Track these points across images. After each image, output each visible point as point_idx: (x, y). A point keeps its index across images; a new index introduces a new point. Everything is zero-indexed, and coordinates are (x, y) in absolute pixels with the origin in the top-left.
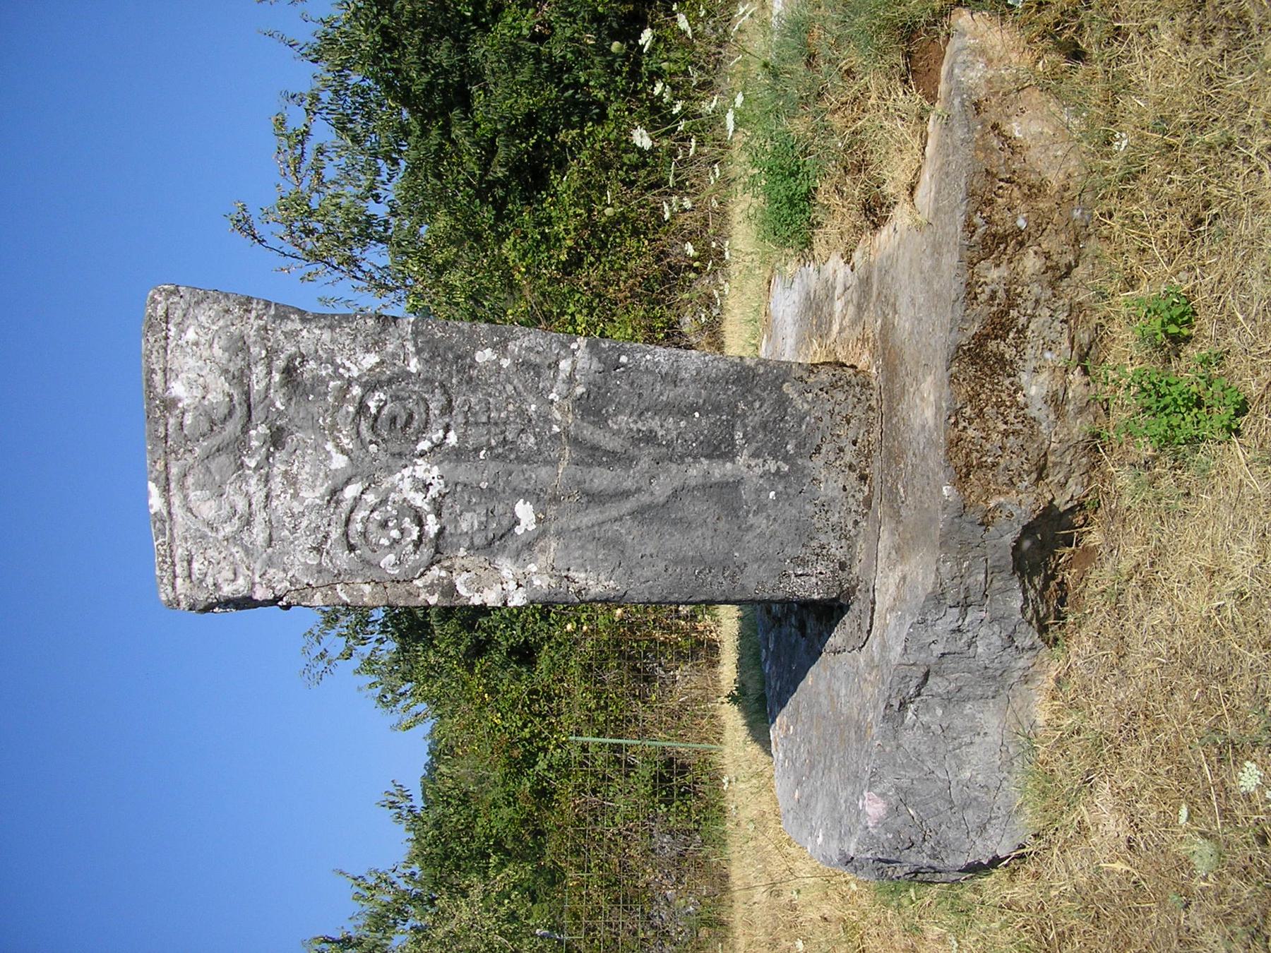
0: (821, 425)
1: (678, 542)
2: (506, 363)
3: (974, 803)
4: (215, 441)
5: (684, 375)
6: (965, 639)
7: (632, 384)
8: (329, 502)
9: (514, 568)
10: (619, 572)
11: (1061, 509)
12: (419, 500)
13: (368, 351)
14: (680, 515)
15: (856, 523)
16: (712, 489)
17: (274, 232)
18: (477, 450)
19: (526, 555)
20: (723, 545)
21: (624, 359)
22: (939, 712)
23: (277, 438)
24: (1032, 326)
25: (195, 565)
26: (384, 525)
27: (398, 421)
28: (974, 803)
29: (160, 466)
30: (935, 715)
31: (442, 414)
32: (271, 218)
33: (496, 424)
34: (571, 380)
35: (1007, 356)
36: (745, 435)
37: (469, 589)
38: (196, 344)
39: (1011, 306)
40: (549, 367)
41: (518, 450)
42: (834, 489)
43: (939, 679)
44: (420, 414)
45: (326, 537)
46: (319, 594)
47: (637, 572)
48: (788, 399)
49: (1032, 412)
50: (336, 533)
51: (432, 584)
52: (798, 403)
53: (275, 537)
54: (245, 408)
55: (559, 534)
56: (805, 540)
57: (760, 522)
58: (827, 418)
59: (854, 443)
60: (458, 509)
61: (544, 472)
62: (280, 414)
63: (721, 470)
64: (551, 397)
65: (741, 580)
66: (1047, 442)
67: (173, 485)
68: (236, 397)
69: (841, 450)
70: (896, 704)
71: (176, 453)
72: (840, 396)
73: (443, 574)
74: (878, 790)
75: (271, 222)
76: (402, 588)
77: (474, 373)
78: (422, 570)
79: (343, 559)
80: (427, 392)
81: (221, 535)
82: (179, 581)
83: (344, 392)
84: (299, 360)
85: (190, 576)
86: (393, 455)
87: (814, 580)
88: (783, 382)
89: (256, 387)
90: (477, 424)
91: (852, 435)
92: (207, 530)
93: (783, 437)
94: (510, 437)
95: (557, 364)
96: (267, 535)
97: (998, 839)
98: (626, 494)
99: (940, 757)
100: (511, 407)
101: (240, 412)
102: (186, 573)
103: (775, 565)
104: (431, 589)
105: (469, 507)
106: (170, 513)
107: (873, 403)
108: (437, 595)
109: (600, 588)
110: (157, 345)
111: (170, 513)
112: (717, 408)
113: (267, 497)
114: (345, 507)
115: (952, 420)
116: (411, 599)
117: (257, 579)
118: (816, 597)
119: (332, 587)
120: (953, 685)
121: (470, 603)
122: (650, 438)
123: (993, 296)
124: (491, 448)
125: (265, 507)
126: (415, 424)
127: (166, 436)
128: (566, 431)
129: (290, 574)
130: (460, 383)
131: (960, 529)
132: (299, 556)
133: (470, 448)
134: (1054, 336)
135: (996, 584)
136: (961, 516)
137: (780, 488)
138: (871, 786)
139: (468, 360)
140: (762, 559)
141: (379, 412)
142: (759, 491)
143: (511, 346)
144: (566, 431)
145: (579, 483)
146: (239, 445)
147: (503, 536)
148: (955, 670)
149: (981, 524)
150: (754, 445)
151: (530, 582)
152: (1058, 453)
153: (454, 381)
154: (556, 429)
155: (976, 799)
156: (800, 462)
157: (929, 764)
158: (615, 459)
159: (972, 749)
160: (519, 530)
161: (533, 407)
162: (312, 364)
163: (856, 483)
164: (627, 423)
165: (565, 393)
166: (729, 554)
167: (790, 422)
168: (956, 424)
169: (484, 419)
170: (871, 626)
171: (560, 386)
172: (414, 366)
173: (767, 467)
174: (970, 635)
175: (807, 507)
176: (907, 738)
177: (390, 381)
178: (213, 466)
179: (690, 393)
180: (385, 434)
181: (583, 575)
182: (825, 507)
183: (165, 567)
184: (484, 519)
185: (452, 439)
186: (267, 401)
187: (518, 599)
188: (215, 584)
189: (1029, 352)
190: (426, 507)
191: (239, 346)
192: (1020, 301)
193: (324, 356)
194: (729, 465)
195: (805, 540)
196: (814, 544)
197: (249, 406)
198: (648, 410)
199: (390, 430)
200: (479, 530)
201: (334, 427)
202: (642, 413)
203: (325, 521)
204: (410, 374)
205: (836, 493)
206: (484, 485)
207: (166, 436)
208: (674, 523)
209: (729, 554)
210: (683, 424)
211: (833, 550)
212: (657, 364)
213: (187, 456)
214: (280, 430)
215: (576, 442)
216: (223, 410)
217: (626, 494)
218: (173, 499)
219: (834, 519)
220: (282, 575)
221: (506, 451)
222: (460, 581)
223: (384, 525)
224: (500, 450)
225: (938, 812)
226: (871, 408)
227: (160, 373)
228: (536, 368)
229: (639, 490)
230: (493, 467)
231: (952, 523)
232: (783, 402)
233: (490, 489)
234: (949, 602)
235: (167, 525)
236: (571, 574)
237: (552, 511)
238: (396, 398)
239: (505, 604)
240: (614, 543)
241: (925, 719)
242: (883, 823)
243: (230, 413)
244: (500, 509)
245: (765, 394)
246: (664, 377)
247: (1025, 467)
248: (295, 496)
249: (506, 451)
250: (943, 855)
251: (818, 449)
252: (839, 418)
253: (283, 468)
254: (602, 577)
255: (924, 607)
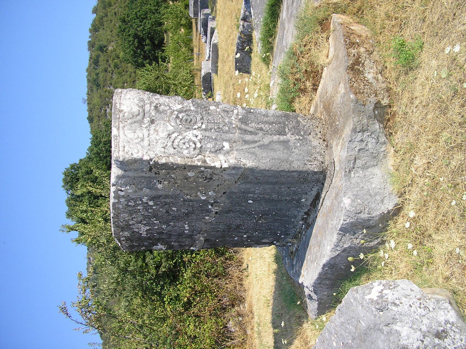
0: (310, 128)
1: (272, 154)
2: (218, 110)
3: (378, 194)
4: (134, 120)
5: (269, 115)
6: (365, 143)
7: (255, 116)
8: (167, 137)
9: (224, 158)
10: (255, 161)
11: (384, 105)
12: (194, 139)
13: (179, 104)
14: (272, 148)
15: (324, 152)
16: (280, 142)
17: (76, 314)
18: (211, 129)
19: (227, 155)
20: (286, 156)
21: (252, 111)
22: (361, 172)
23: (152, 122)
24: (366, 63)
25: (126, 148)
26: (184, 144)
27: (188, 121)
28: (378, 194)
29: (117, 124)
30: (360, 173)
31: (201, 119)
32: (75, 305)
33: (216, 123)
34: (237, 114)
35: (361, 70)
36: (289, 130)
37: (210, 162)
38: (130, 99)
39: (359, 58)
40: (231, 111)
41: (223, 130)
42: (316, 143)
43: (359, 160)
44: (194, 119)
45: (167, 145)
46: (164, 158)
47: (261, 161)
48: (299, 121)
49: (370, 81)
50: (170, 144)
51: (199, 159)
52: (303, 122)
53: (150, 144)
54: (143, 113)
55: (237, 150)
56: (310, 156)
57: (296, 151)
58: (311, 126)
59: (320, 132)
60: (206, 142)
61: (231, 135)
62: (153, 116)
63: (282, 138)
64: (232, 118)
65: (293, 165)
66: (376, 88)
67: (120, 129)
68: (141, 111)
69: (317, 134)
70: (347, 170)
71: (122, 122)
72: (314, 121)
73: (202, 157)
74: (347, 196)
75: (75, 307)
76: (189, 160)
77: (210, 111)
78: (196, 155)
79: (172, 151)
80: (196, 114)
81: (134, 142)
82: (120, 152)
83: (172, 113)
84: (159, 105)
85: (124, 151)
86: (187, 128)
87: (314, 166)
88: (298, 117)
89: (146, 109)
90: (211, 123)
91: (319, 130)
92: (130, 141)
93: (300, 130)
94: (221, 127)
95: (233, 111)
96: (148, 143)
97: (388, 203)
98: (256, 142)
99: (364, 183)
100: (220, 120)
101: (142, 114)
102: (123, 150)
103: (302, 162)
104: (199, 160)
105: (209, 142)
106: (119, 135)
107: (324, 123)
108: (200, 162)
109: (250, 165)
110: (118, 98)
111: (119, 135)
112: (280, 123)
113: (149, 134)
114: (172, 139)
115: (350, 82)
116: (192, 163)
117: (145, 154)
118: (316, 170)
119: (168, 157)
120: (364, 162)
121: (211, 165)
122: (261, 129)
123: (354, 55)
124: (215, 129)
125: (148, 137)
126: (193, 122)
127: (119, 118)
128: (237, 126)
129: (155, 153)
130: (206, 113)
131: (357, 107)
132: (158, 148)
133: (209, 128)
134: (372, 66)
135: (370, 123)
136: (357, 103)
137: (301, 142)
138: (345, 196)
139: (208, 108)
140: (298, 160)
141: (182, 118)
142: (295, 143)
143: (220, 106)
144: (237, 126)
145: (242, 138)
146: (141, 122)
147: (220, 150)
148: (364, 157)
149: (363, 105)
150: (291, 132)
151: (229, 161)
152: (379, 91)
153: (204, 113)
154: (234, 126)
155: (378, 192)
156: (305, 136)
157: (362, 185)
158: (251, 133)
159: (374, 179)
160: (224, 149)
161: (227, 120)
162: (163, 107)
163: (322, 142)
164: (254, 125)
165: (236, 117)
166: (288, 158)
167: (301, 127)
168: (351, 83)
169: (213, 122)
170: (335, 168)
171: (234, 116)
172: (192, 108)
173: (296, 137)
174: (366, 142)
175: (309, 147)
176: (353, 181)
177: (186, 111)
178: (133, 126)
179: (272, 119)
180: (184, 123)
181: (245, 161)
182: (314, 147)
183: (117, 148)
184: (214, 145)
185: (204, 126)
186: (150, 113)
187: (225, 165)
188: (132, 154)
189: (366, 69)
190: (197, 141)
191: (142, 100)
192: (361, 57)
193: (166, 104)
194: (285, 137)
195: (310, 156)
196: (313, 157)
197: (144, 113)
198: (260, 122)
199: (186, 122)
200: (213, 147)
201: (169, 121)
202: (258, 123)
203: (166, 142)
204: (191, 110)
205: (317, 144)
206: (214, 137)
207: (119, 118)
208: (271, 150)
209: (288, 158)
210: (270, 126)
211: (319, 159)
212: (262, 112)
213: (125, 123)
214: (153, 120)
215: (240, 129)
216: (137, 113)
217: (256, 142)
218: (120, 132)
219: (318, 150)
220: (153, 153)
221: (219, 130)
222: (208, 160)
223: (184, 144)
224: (218, 130)
225: (367, 199)
226: (323, 124)
227: (119, 104)
228: (227, 112)
229: (259, 141)
230: (216, 133)
231: (355, 106)
232: (298, 122)
233: (215, 139)
234: (358, 130)
235: (118, 138)
236: (241, 160)
237: (234, 145)
238: (188, 115)
239: (221, 167)
240: (253, 153)
241: (357, 175)
242: (351, 205)
243: (139, 114)
244: (218, 143)
245: (293, 120)
246: (264, 115)
247: (372, 92)
248: (157, 134)
249: (219, 130)
250: (372, 213)
251: (310, 134)
252: (315, 127)
253: (154, 128)
254: (251, 162)
255: (351, 135)
